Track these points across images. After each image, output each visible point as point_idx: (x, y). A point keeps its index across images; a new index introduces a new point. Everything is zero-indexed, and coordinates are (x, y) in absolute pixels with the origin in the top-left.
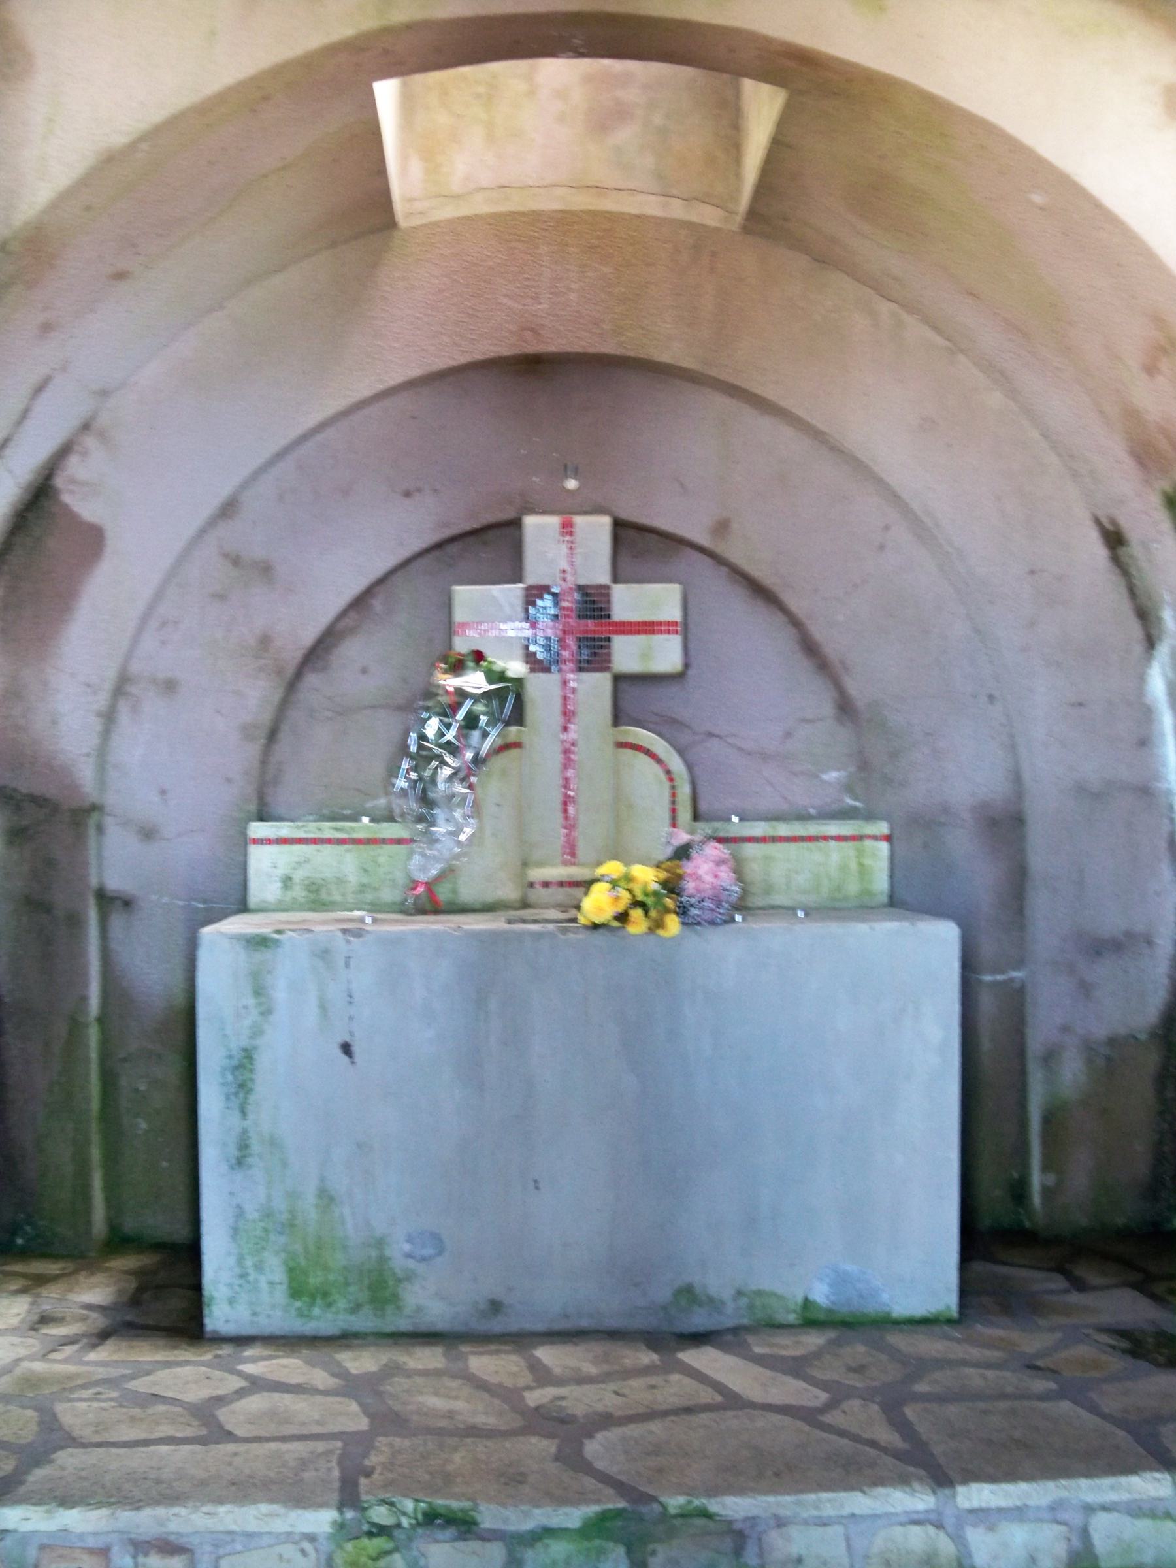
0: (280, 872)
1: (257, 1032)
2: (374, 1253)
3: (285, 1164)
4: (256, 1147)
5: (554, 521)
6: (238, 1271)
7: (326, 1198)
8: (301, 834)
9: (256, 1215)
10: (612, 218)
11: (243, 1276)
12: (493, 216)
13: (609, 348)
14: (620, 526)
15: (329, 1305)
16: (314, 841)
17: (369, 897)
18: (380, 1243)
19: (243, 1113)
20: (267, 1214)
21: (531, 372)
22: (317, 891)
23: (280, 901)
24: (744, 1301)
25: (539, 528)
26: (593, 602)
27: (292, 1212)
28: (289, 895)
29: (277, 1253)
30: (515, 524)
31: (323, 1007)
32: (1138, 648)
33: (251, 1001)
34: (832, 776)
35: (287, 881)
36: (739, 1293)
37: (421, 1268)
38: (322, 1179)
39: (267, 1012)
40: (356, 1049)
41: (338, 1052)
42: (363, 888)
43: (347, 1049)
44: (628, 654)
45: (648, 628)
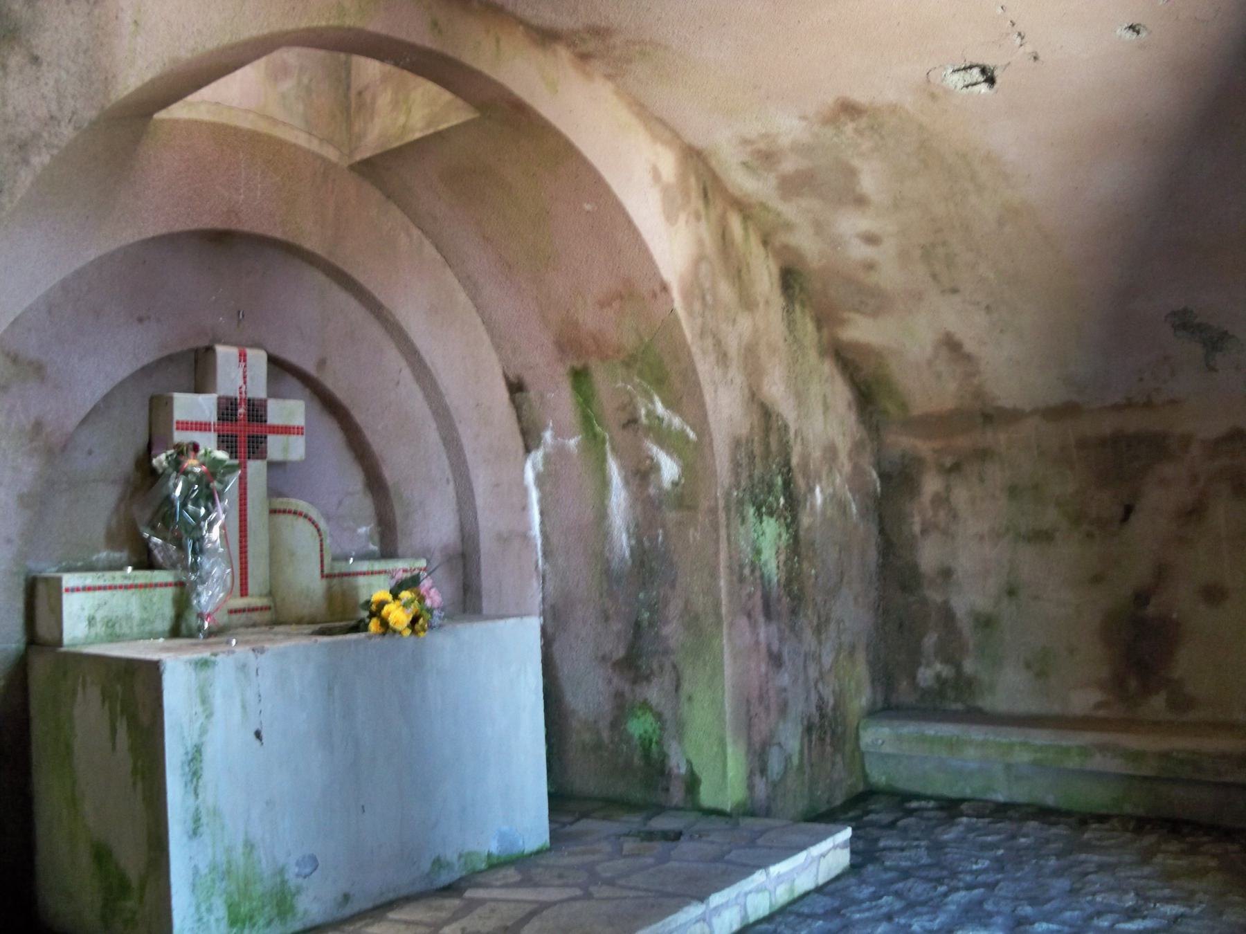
0: (86, 613)
1: (203, 731)
2: (279, 879)
3: (223, 827)
4: (204, 820)
5: (234, 351)
6: (196, 917)
7: (250, 846)
8: (101, 583)
9: (207, 871)
10: (281, 143)
11: (200, 920)
12: (214, 124)
13: (278, 234)
14: (273, 361)
15: (254, 925)
16: (110, 588)
17: (147, 628)
18: (282, 871)
19: (196, 795)
20: (213, 868)
21: (221, 241)
22: (113, 626)
23: (87, 637)
24: (463, 860)
25: (225, 354)
26: (256, 411)
27: (229, 862)
28: (93, 631)
29: (221, 895)
30: (210, 350)
31: (244, 707)
32: (521, 451)
33: (199, 709)
34: (363, 530)
35: (91, 621)
36: (460, 856)
37: (305, 883)
38: (246, 833)
39: (209, 716)
40: (264, 734)
41: (253, 737)
42: (143, 622)
43: (258, 735)
44: (275, 447)
45: (286, 430)
